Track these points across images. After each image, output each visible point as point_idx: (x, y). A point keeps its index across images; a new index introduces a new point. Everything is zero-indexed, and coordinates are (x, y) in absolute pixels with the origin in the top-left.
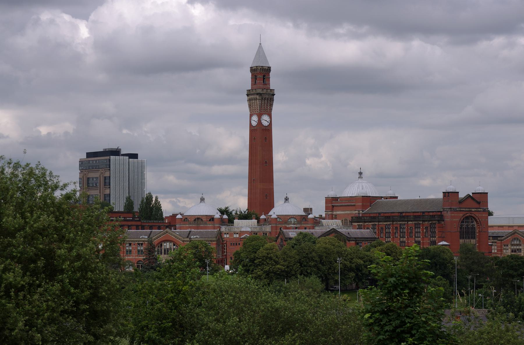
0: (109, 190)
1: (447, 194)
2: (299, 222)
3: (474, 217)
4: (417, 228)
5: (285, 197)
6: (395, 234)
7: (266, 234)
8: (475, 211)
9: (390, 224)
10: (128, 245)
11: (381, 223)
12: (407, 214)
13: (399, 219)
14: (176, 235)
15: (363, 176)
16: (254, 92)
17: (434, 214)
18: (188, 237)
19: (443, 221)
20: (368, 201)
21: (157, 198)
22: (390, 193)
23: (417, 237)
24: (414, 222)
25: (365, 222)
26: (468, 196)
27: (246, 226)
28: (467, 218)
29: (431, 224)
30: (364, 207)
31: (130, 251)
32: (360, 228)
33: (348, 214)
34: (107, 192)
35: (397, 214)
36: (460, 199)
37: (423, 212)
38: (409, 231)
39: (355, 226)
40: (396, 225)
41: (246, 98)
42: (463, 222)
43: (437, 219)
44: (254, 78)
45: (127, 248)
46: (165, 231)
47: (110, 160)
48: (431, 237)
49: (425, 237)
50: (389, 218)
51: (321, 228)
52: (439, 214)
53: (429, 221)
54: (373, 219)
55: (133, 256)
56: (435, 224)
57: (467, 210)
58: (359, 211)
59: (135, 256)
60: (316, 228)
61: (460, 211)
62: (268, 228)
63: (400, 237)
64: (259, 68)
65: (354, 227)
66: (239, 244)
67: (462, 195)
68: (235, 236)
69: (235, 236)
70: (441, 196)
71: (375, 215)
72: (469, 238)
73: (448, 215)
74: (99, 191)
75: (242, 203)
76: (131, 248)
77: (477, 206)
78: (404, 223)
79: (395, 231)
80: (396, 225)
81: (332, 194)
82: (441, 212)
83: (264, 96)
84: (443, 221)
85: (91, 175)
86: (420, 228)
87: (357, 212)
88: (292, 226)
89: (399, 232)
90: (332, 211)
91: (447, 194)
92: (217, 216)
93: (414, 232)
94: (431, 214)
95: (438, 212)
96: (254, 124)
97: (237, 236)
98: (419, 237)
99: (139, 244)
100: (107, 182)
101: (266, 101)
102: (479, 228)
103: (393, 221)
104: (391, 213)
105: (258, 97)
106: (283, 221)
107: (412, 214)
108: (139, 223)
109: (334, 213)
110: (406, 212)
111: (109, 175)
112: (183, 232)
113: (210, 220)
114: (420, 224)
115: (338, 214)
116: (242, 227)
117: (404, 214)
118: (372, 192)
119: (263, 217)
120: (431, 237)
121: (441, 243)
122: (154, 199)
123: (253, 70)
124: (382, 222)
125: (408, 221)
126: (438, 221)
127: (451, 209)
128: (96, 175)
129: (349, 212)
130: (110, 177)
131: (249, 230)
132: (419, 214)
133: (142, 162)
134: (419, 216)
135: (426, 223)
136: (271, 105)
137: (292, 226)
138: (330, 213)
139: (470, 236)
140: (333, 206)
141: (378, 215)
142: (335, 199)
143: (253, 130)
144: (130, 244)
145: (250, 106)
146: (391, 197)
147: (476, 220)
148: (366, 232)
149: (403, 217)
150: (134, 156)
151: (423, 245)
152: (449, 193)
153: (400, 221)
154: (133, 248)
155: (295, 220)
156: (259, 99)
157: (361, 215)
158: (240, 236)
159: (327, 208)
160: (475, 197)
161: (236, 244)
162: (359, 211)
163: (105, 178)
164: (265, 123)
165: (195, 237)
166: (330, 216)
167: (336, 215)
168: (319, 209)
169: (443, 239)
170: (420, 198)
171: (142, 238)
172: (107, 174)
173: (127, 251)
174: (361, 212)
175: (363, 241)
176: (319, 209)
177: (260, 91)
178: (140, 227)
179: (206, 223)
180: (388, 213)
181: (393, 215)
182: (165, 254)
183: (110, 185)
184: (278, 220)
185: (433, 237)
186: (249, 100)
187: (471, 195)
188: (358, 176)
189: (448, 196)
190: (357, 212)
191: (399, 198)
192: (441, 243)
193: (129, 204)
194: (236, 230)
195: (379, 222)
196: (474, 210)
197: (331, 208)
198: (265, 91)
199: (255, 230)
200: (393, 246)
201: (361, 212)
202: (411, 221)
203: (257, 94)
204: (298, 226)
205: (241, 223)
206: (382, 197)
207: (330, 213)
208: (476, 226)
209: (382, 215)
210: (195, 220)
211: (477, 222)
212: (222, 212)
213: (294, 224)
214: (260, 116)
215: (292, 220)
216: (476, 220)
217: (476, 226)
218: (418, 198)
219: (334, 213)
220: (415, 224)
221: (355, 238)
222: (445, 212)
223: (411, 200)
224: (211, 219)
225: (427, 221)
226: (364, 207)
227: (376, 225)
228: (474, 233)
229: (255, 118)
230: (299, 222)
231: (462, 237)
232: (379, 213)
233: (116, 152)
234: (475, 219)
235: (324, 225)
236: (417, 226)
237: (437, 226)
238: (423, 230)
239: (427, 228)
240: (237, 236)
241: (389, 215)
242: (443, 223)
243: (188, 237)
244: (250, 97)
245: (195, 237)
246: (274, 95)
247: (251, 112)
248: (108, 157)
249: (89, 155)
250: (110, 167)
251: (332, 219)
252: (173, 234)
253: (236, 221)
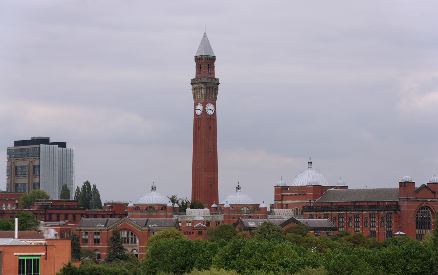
0: (38, 179)
1: (403, 184)
2: (252, 211)
3: (429, 208)
4: (372, 217)
5: (237, 185)
6: (349, 224)
7: (219, 223)
8: (430, 201)
9: (343, 214)
10: (84, 234)
11: (334, 213)
12: (361, 204)
13: (353, 209)
14: (134, 224)
15: (313, 165)
16: (199, 81)
17: (390, 203)
18: (145, 226)
19: (400, 211)
20: (319, 190)
21: (94, 186)
22: (340, 183)
23: (372, 227)
24: (369, 212)
25: (317, 211)
26: (424, 186)
27: (198, 215)
28: (423, 208)
29: (387, 214)
30: (315, 196)
31: (99, 240)
32: (311, 217)
33: (299, 204)
34: (37, 180)
35: (350, 204)
36: (416, 189)
37: (378, 202)
38: (364, 221)
39: (307, 215)
40: (350, 215)
41: (191, 87)
42: (418, 212)
43: (393, 209)
44: (199, 67)
45: (83, 237)
46: (123, 219)
47: (39, 148)
48: (387, 227)
49: (381, 227)
50: (342, 207)
51: (273, 217)
52: (395, 203)
53: (385, 211)
54: (326, 208)
55: (89, 245)
56: (391, 213)
57: (423, 200)
58: (310, 200)
59: (92, 245)
60: (269, 217)
61: (417, 201)
62: (220, 217)
63: (355, 227)
64: (204, 57)
65: (305, 217)
66: (193, 233)
67: (418, 185)
68: (187, 225)
69: (187, 225)
70: (397, 186)
71: (327, 205)
72: (424, 228)
73: (404, 206)
74: (28, 179)
75: (185, 194)
76: (87, 237)
77: (433, 196)
78: (358, 212)
79: (348, 221)
80: (350, 215)
81: (281, 183)
82: (397, 202)
83: (209, 85)
84: (400, 211)
85: (20, 163)
86: (375, 217)
87: (308, 201)
88: (246, 215)
89: (353, 222)
90: (282, 200)
91: (403, 184)
92: (170, 205)
93: (369, 222)
94: (386, 203)
95: (394, 201)
96: (199, 113)
97: (190, 225)
98: (374, 227)
99: (95, 233)
100: (36, 169)
101: (211, 90)
102: (434, 218)
103: (347, 211)
104: (344, 202)
105: (203, 86)
106: (235, 210)
107: (366, 204)
108: (83, 212)
109: (284, 202)
110: (360, 202)
111: (38, 164)
112: (140, 220)
113: (162, 209)
114: (375, 213)
115: (290, 204)
116: (194, 216)
117: (357, 204)
118: (322, 180)
119: (214, 206)
120: (387, 227)
121: (398, 233)
122: (92, 187)
123: (198, 59)
124: (335, 211)
125: (362, 211)
126: (395, 210)
127: (407, 198)
128: (25, 163)
129: (299, 201)
130: (39, 166)
131: (201, 218)
132: (374, 204)
133: (71, 151)
134: (374, 206)
135: (381, 212)
136: (216, 94)
137: (246, 215)
138: (279, 202)
139: (426, 226)
140: (283, 196)
141: (330, 204)
142: (285, 188)
143: (197, 119)
144: (86, 233)
145: (194, 95)
146: (341, 187)
147: (431, 210)
148: (322, 221)
149: (357, 206)
150: (62, 145)
151: (379, 235)
152: (405, 182)
153: (354, 211)
154: (89, 237)
155: (248, 209)
156: (204, 88)
157: (312, 205)
158: (192, 224)
159: (276, 197)
160: (429, 186)
161: (190, 233)
162: (310, 200)
163: (35, 167)
164: (210, 112)
165: (153, 226)
166: (280, 206)
167: (287, 205)
168: (267, 200)
169: (399, 229)
170: (367, 188)
171: (99, 227)
172: (36, 163)
173: (83, 240)
174: (312, 201)
175: (322, 230)
176: (267, 200)
177: (204, 80)
178: (85, 216)
179: (158, 212)
180: (373, 202)
181: (345, 204)
182: (132, 243)
183: (39, 173)
184: (231, 208)
185: (389, 227)
186: (194, 89)
187: (426, 184)
188: (307, 165)
189: (405, 186)
190: (308, 201)
191: (349, 188)
192: (398, 233)
193: (65, 192)
194: (188, 219)
195: (332, 211)
196: (429, 200)
197: (280, 197)
198: (210, 80)
199: (208, 219)
200: (361, 236)
201: (312, 201)
202: (366, 211)
203: (202, 83)
204: (251, 215)
205: (193, 212)
206: (332, 187)
207: (279, 202)
208: (431, 216)
209: (334, 204)
210: (147, 209)
211: (432, 212)
212: (173, 200)
213: (247, 213)
214: (204, 106)
215: (245, 209)
216: (431, 210)
217: (431, 216)
218: (365, 188)
219: (284, 202)
220: (370, 214)
221: (314, 228)
222: (402, 202)
223: (391, 189)
224: (164, 207)
225: (382, 211)
226: (315, 196)
227: (328, 214)
228: (429, 223)
229: (200, 107)
230: (252, 211)
231: (418, 227)
232: (332, 203)
233: (46, 141)
234: (430, 209)
235: (276, 214)
236: (372, 216)
237: (393, 216)
238: (378, 221)
239: (382, 218)
240: (190, 225)
241: (342, 204)
242: (399, 212)
243: (145, 226)
244: (195, 86)
245: (153, 226)
246: (218, 84)
247: (195, 101)
248: (38, 146)
249: (17, 143)
250: (39, 156)
251: (282, 208)
252: (131, 222)
253: (188, 210)
